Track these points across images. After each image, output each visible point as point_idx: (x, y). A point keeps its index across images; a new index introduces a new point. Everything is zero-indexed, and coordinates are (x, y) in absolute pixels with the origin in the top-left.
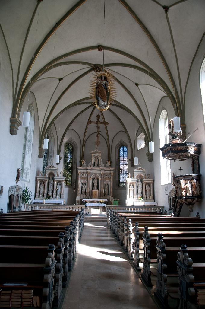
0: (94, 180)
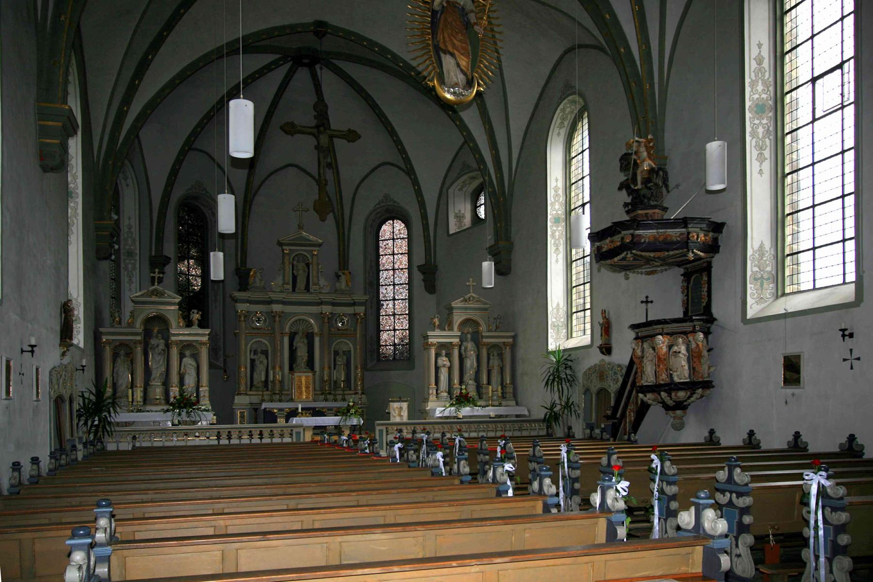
0: (297, 338)
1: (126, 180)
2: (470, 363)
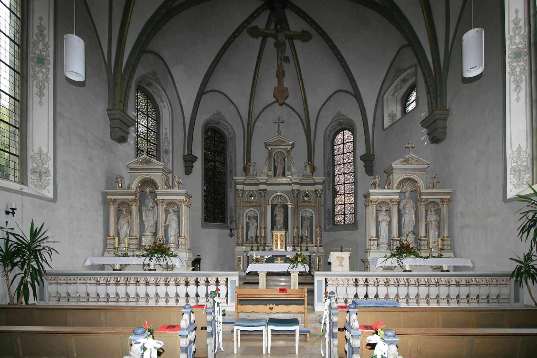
0: (277, 208)
1: (163, 103)
2: (409, 217)
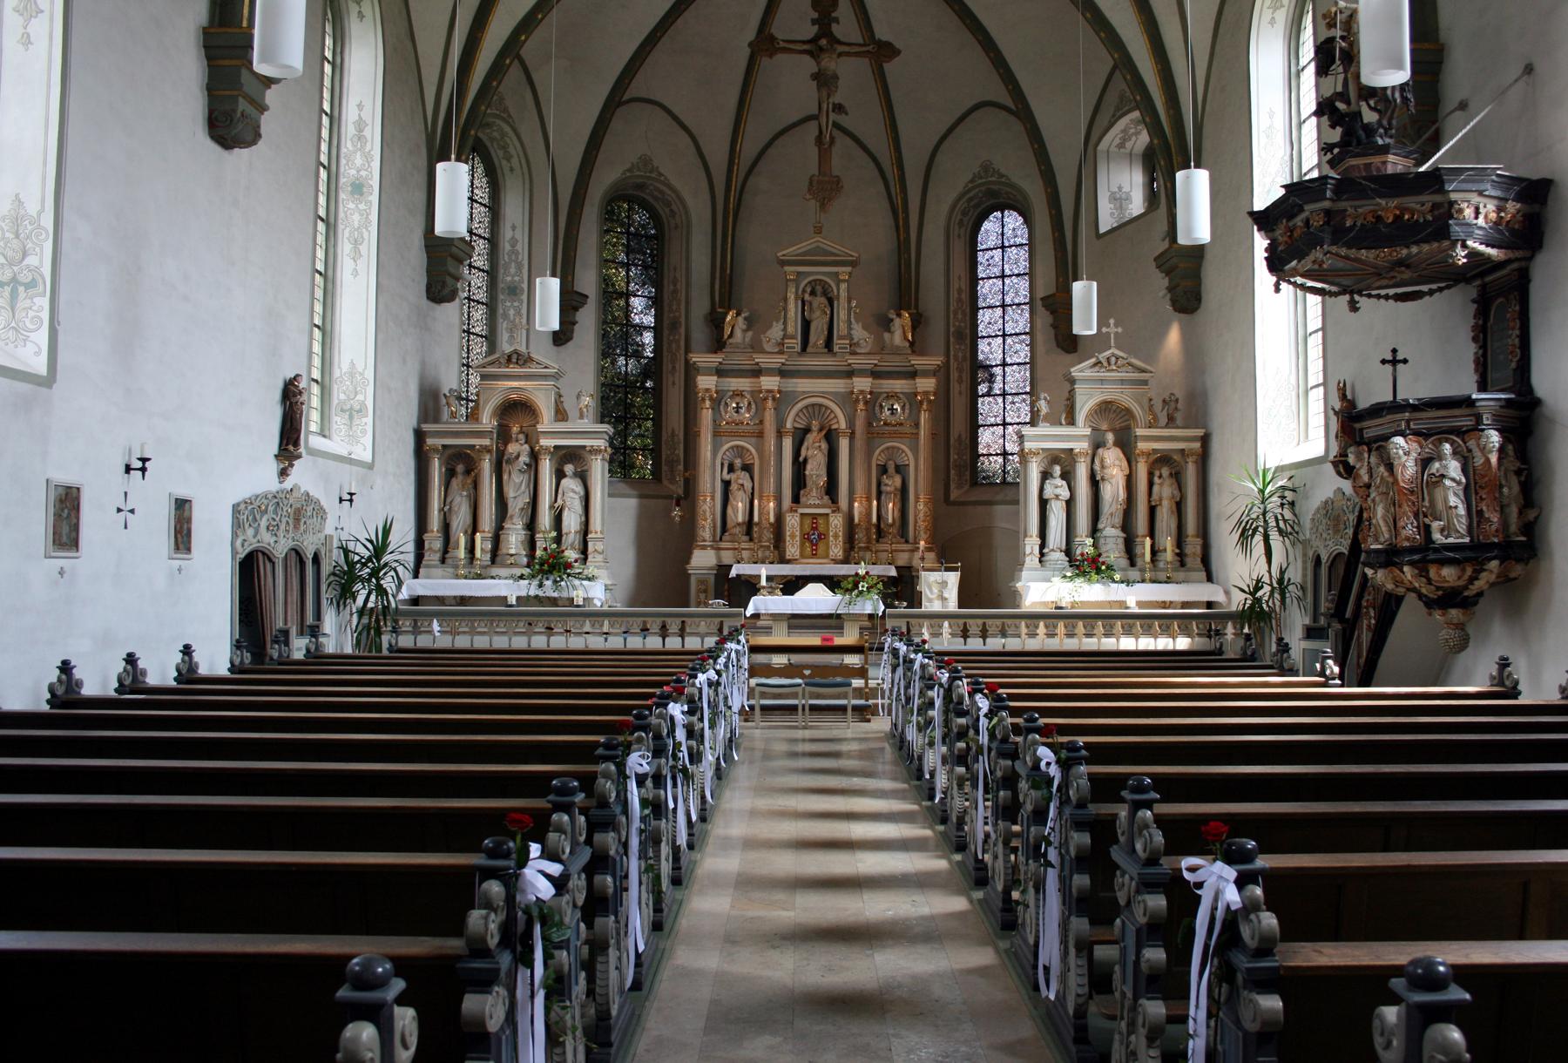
0: (810, 438)
1: (508, 160)
